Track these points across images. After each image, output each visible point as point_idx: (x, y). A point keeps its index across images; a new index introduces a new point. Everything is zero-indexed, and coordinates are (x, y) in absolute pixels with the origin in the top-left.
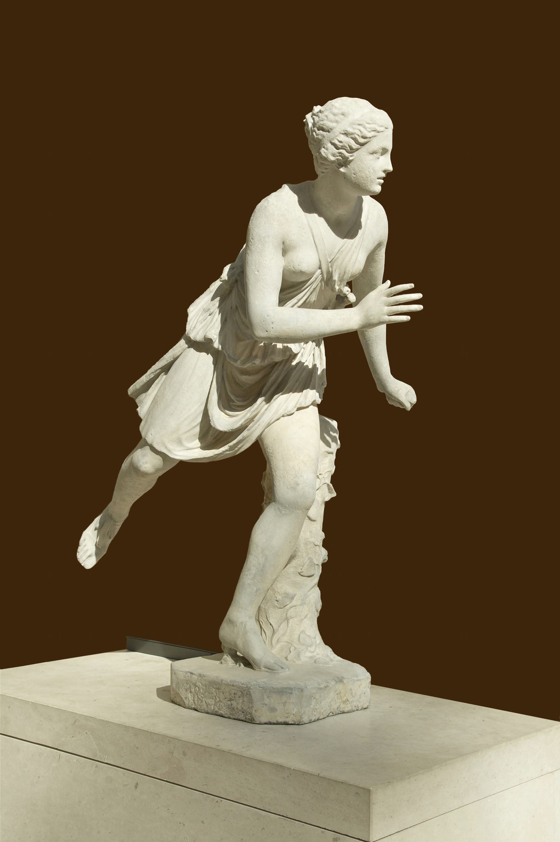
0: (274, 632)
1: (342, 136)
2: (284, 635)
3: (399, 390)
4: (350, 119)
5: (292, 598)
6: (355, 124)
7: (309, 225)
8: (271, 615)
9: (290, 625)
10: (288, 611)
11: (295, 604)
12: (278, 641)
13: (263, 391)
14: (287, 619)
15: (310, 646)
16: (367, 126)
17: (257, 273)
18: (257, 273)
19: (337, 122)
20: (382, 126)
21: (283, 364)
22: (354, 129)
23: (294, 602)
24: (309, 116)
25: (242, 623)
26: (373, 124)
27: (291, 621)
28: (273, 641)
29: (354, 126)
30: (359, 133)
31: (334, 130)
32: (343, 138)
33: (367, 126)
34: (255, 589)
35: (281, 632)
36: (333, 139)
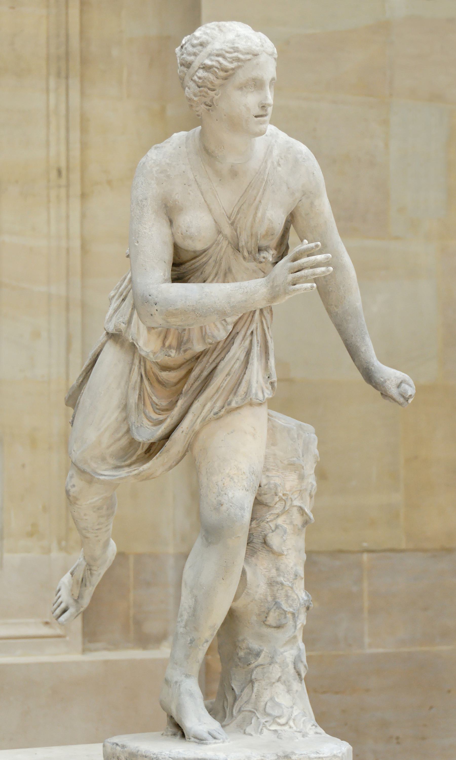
0: (235, 699)
1: (201, 71)
2: (247, 702)
3: (385, 381)
4: (209, 49)
5: (258, 655)
6: (213, 55)
7: (196, 180)
8: (233, 677)
9: (255, 690)
10: (252, 671)
11: (262, 663)
12: (240, 711)
13: (184, 390)
14: (252, 682)
15: (279, 717)
16: (228, 55)
17: (136, 244)
18: (136, 244)
19: (195, 54)
20: (248, 53)
21: (209, 354)
22: (212, 60)
23: (260, 660)
24: (178, 50)
25: (176, 682)
26: (235, 52)
27: (256, 685)
28: (234, 711)
29: (213, 58)
30: (218, 65)
31: (193, 65)
32: (201, 73)
33: (228, 55)
34: (189, 639)
35: (244, 697)
36: (193, 76)
